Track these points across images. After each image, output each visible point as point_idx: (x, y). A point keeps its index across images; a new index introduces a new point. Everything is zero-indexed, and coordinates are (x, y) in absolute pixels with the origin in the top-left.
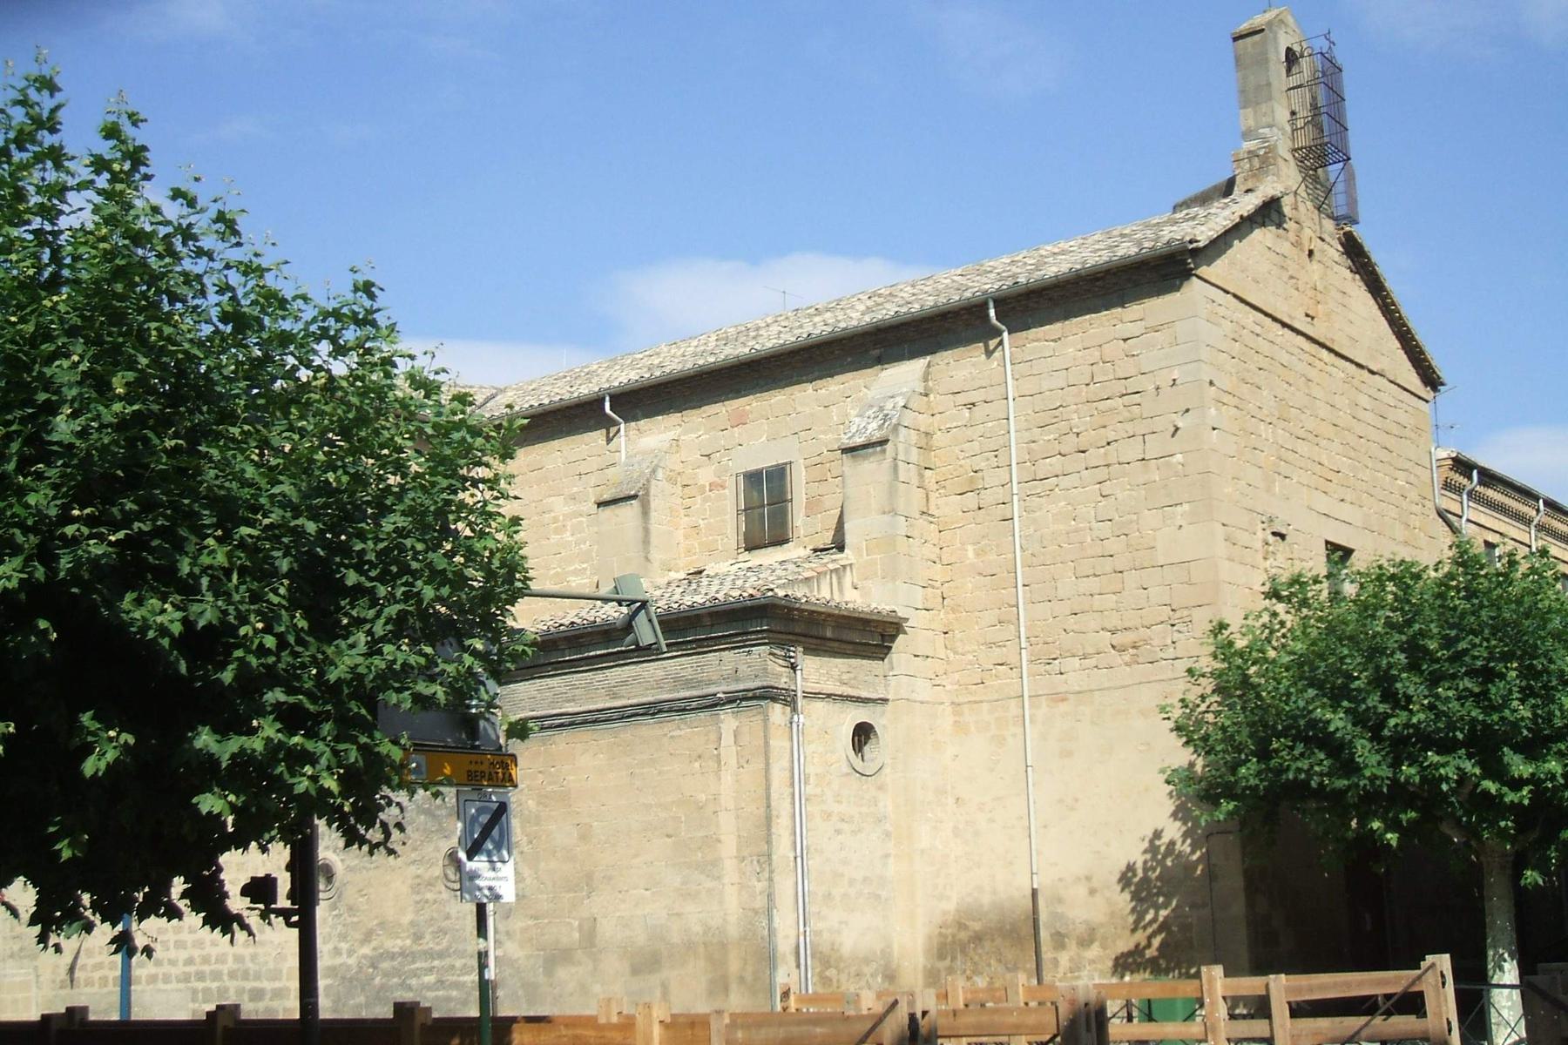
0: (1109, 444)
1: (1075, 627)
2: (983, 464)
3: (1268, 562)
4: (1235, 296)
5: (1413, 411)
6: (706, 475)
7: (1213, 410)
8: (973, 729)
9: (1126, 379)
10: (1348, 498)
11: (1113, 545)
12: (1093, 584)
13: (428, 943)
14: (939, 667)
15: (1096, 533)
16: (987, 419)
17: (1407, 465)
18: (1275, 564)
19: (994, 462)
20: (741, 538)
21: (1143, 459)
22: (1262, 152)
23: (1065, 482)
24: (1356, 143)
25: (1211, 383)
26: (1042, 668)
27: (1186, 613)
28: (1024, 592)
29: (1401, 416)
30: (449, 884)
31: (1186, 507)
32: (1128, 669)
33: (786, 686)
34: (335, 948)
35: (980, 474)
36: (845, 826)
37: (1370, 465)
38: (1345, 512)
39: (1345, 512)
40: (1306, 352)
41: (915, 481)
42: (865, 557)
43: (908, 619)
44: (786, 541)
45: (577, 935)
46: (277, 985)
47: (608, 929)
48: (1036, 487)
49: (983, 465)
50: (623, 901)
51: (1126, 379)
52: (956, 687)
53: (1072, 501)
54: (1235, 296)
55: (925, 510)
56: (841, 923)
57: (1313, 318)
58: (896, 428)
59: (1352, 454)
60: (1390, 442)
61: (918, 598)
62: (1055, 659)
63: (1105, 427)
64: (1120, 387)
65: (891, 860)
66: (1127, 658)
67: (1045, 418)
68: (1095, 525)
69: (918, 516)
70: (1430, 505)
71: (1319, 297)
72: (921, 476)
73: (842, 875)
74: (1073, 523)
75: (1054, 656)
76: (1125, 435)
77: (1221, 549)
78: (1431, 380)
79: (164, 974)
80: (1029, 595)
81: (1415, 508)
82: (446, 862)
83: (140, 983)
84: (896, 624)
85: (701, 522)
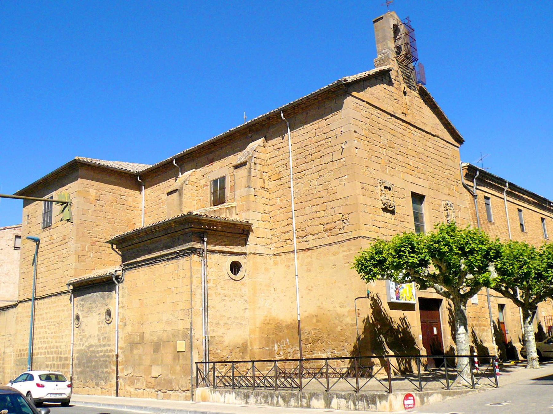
0: (321, 157)
1: (311, 224)
2: (282, 169)
3: (382, 197)
4: (368, 103)
5: (455, 151)
6: (202, 182)
7: (356, 141)
8: (279, 263)
9: (326, 133)
10: (422, 177)
11: (323, 193)
12: (316, 208)
13: (102, 343)
14: (268, 241)
15: (317, 190)
16: (283, 153)
17: (450, 168)
18: (385, 198)
19: (285, 168)
20: (212, 201)
21: (332, 161)
22: (383, 58)
23: (307, 172)
24: (420, 54)
25: (355, 132)
26: (301, 240)
27: (347, 216)
28: (295, 213)
29: (446, 151)
30: (107, 322)
31: (346, 177)
32: (328, 238)
33: (200, 247)
34: (79, 344)
35: (281, 173)
36: (226, 298)
37: (432, 167)
38: (420, 182)
39: (420, 182)
40: (402, 125)
41: (259, 176)
42: (240, 203)
43: (253, 224)
44: (225, 202)
45: (139, 339)
46: (66, 356)
47: (147, 336)
48: (298, 175)
49: (282, 170)
50: (151, 326)
51: (326, 133)
52: (274, 248)
53: (310, 179)
54: (368, 103)
55: (263, 186)
56: (224, 333)
57: (406, 115)
58: (251, 158)
59: (424, 162)
60: (442, 160)
61: (259, 217)
62: (305, 236)
63: (320, 151)
64: (324, 136)
65: (247, 311)
66: (328, 234)
67: (301, 150)
68: (317, 186)
69: (260, 188)
70: (460, 182)
71: (408, 107)
72: (262, 175)
73: (224, 316)
74: (310, 186)
75: (305, 235)
76: (326, 153)
77: (359, 191)
78: (460, 141)
79: (53, 354)
80: (297, 214)
81: (453, 183)
82: (106, 314)
83: (35, 355)
84: (249, 226)
85: (201, 198)
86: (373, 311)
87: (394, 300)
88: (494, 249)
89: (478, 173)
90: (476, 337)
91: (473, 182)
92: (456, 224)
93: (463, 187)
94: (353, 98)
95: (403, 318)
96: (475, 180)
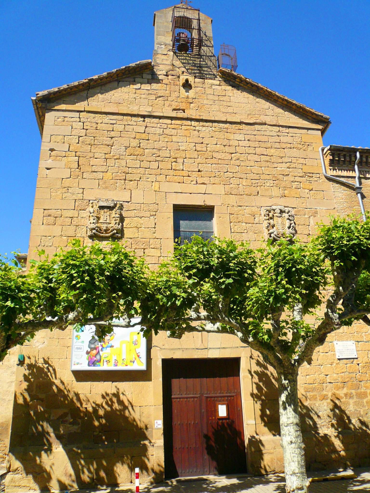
86: (28, 386)
87: (84, 366)
88: (321, 276)
89: (358, 155)
90: (348, 418)
91: (354, 170)
92: (234, 243)
93: (327, 181)
94: (65, 113)
95: (114, 395)
96: (356, 167)
